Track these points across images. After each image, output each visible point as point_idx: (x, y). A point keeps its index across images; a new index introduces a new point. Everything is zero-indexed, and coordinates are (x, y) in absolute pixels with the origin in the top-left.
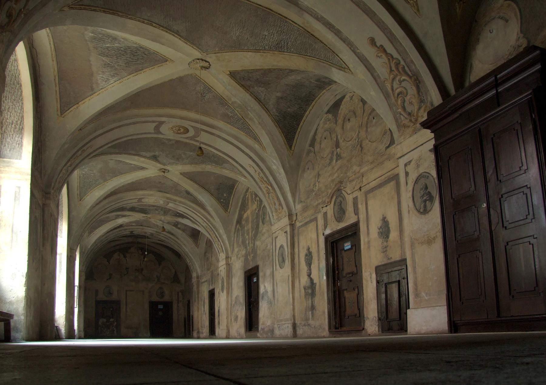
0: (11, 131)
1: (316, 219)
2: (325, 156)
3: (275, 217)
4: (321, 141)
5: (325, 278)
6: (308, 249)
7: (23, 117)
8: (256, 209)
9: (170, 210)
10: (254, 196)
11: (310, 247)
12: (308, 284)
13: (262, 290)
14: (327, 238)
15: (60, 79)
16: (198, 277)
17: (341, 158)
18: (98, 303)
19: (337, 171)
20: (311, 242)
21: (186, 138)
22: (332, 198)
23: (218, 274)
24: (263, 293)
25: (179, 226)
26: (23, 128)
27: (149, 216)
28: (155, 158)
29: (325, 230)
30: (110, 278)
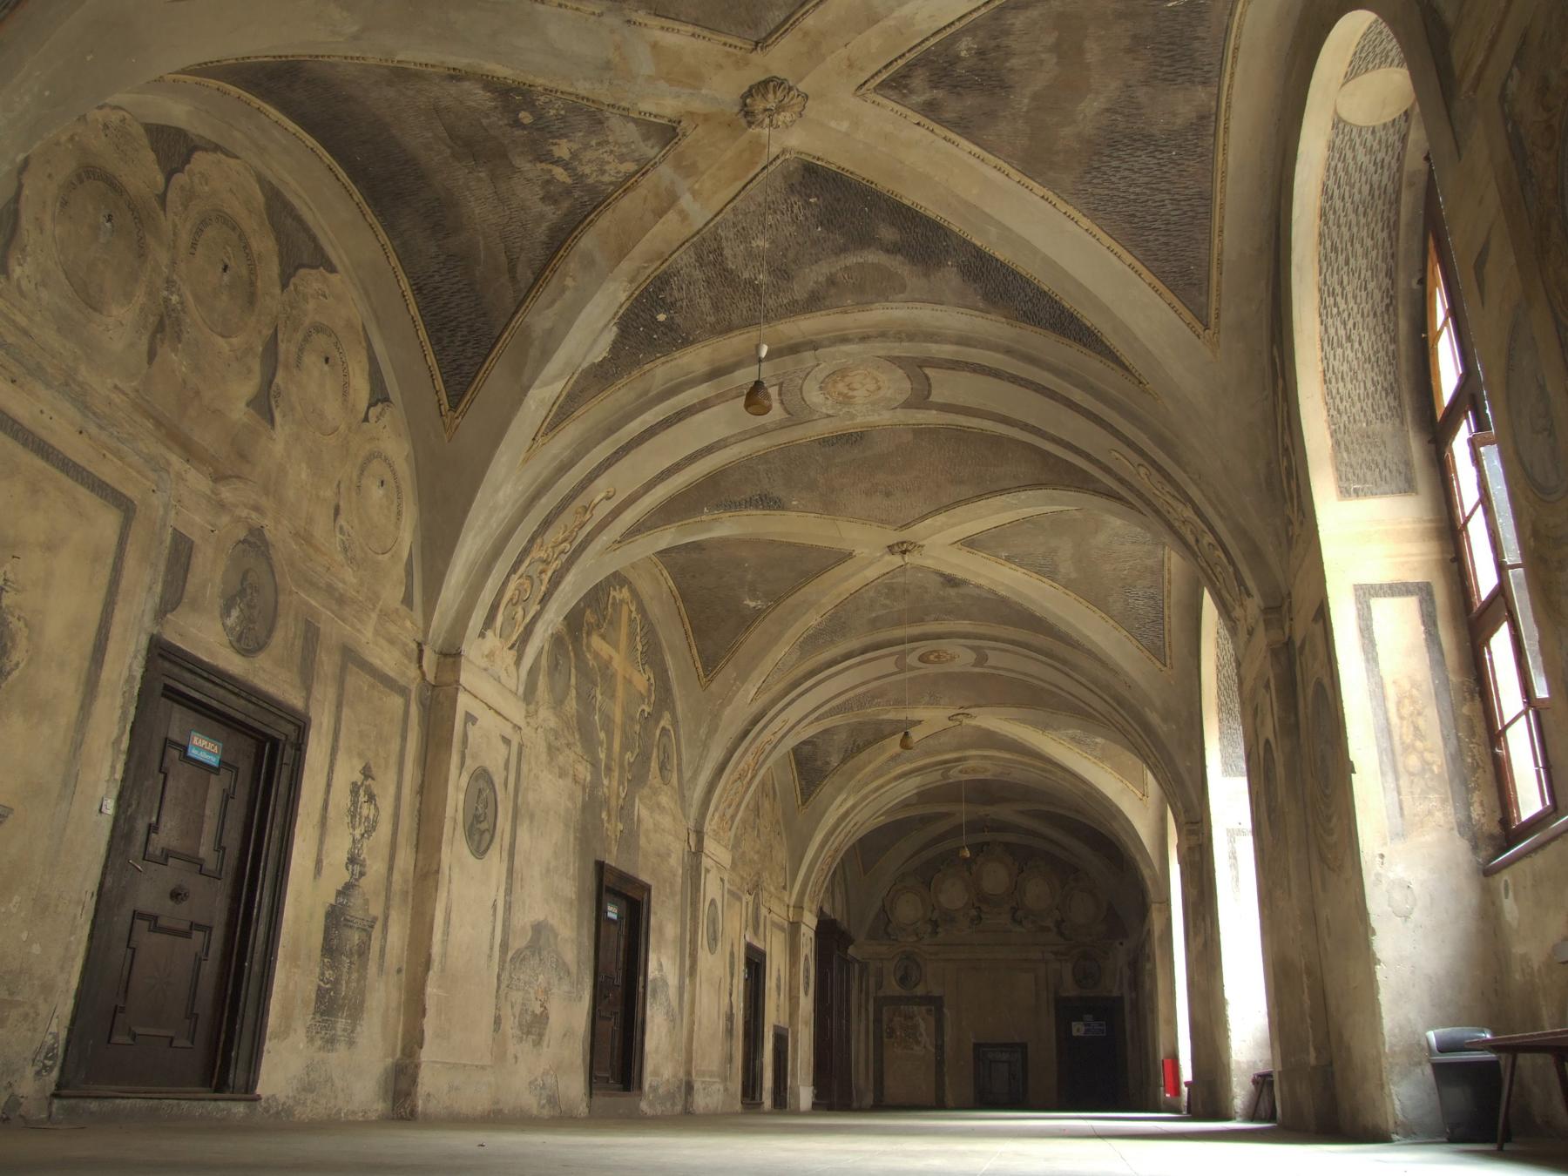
24: (655, 980)
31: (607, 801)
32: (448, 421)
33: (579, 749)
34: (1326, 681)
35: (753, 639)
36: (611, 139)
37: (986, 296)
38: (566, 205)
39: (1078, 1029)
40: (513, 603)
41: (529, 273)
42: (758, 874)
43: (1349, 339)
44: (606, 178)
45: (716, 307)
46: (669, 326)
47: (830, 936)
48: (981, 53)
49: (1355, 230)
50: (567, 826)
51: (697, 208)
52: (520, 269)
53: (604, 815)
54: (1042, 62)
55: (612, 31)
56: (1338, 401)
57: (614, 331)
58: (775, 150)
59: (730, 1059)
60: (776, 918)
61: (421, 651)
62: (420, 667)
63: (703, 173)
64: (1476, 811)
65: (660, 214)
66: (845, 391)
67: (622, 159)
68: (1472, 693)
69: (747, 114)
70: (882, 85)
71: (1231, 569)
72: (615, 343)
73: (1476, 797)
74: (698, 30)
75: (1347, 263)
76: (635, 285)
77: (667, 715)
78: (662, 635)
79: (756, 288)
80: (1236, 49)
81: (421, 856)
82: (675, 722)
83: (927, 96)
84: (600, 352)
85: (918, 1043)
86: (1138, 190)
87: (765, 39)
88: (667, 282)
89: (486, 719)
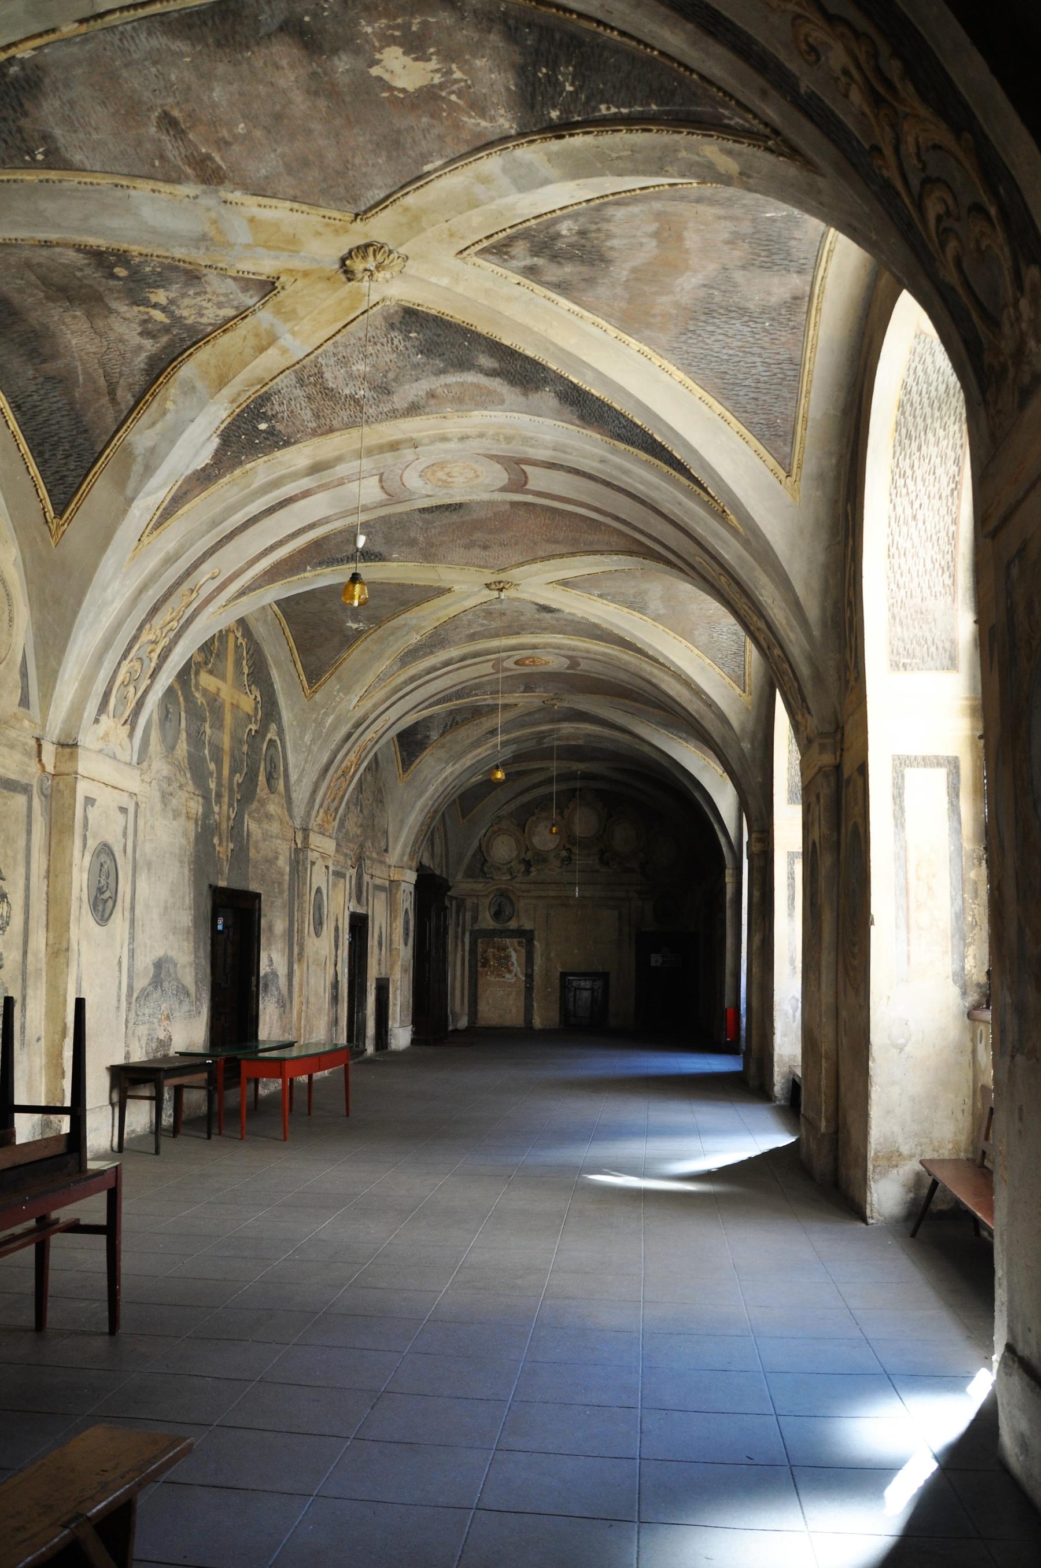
3: (319, 821)
13: (264, 968)
18: (216, 892)
24: (266, 975)
31: (218, 826)
32: (53, 527)
33: (191, 787)
34: (862, 830)
35: (355, 655)
36: (209, 289)
37: (582, 417)
38: (165, 339)
39: (656, 960)
40: (125, 685)
41: (129, 396)
42: (362, 846)
43: (914, 517)
44: (204, 320)
45: (317, 417)
46: (271, 432)
47: (430, 891)
48: (582, 233)
49: (929, 421)
50: (181, 862)
51: (296, 341)
52: (119, 393)
53: (216, 841)
54: (641, 244)
55: (208, 210)
56: (898, 576)
57: (216, 441)
58: (375, 298)
59: (336, 1022)
60: (378, 881)
61: (40, 746)
62: (40, 760)
63: (302, 319)
64: (970, 963)
65: (262, 350)
66: (444, 477)
67: (220, 305)
68: (980, 860)
69: (346, 272)
70: (484, 251)
71: (796, 685)
72: (217, 451)
73: (971, 951)
74: (296, 206)
75: (919, 449)
76: (235, 405)
77: (273, 727)
78: (268, 651)
79: (357, 402)
80: (830, 251)
81: (51, 935)
82: (281, 732)
83: (529, 261)
84: (204, 458)
85: (510, 972)
86: (731, 352)
87: (365, 212)
88: (268, 399)
89: (107, 799)
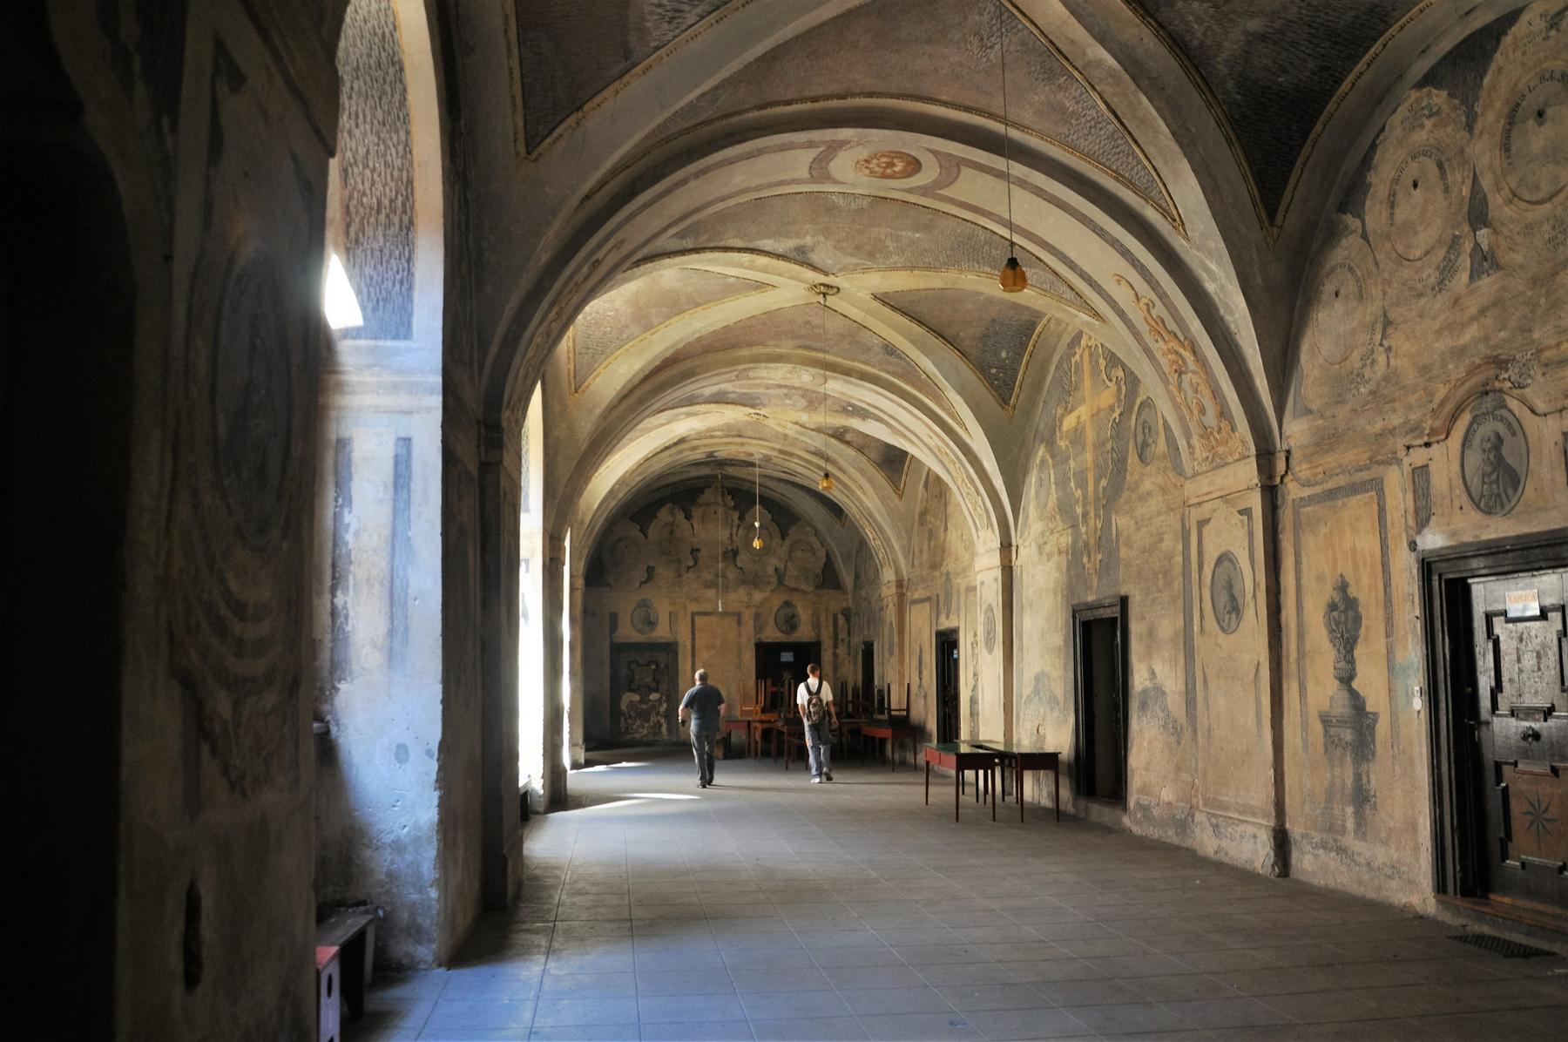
0: (375, 238)
1: (1377, 486)
2: (1417, 253)
4: (1392, 194)
5: (1418, 703)
6: (1343, 587)
7: (410, 182)
8: (1112, 408)
9: (826, 397)
10: (1102, 362)
11: (1349, 578)
12: (1342, 708)
13: (1139, 679)
14: (1427, 567)
15: (524, 27)
16: (900, 584)
17: (1497, 266)
19: (1473, 319)
20: (1355, 565)
21: (909, 191)
22: (1454, 418)
23: (971, 589)
24: (1144, 691)
25: (848, 437)
26: (411, 222)
27: (763, 412)
28: (801, 257)
29: (1419, 532)
30: (649, 580)
